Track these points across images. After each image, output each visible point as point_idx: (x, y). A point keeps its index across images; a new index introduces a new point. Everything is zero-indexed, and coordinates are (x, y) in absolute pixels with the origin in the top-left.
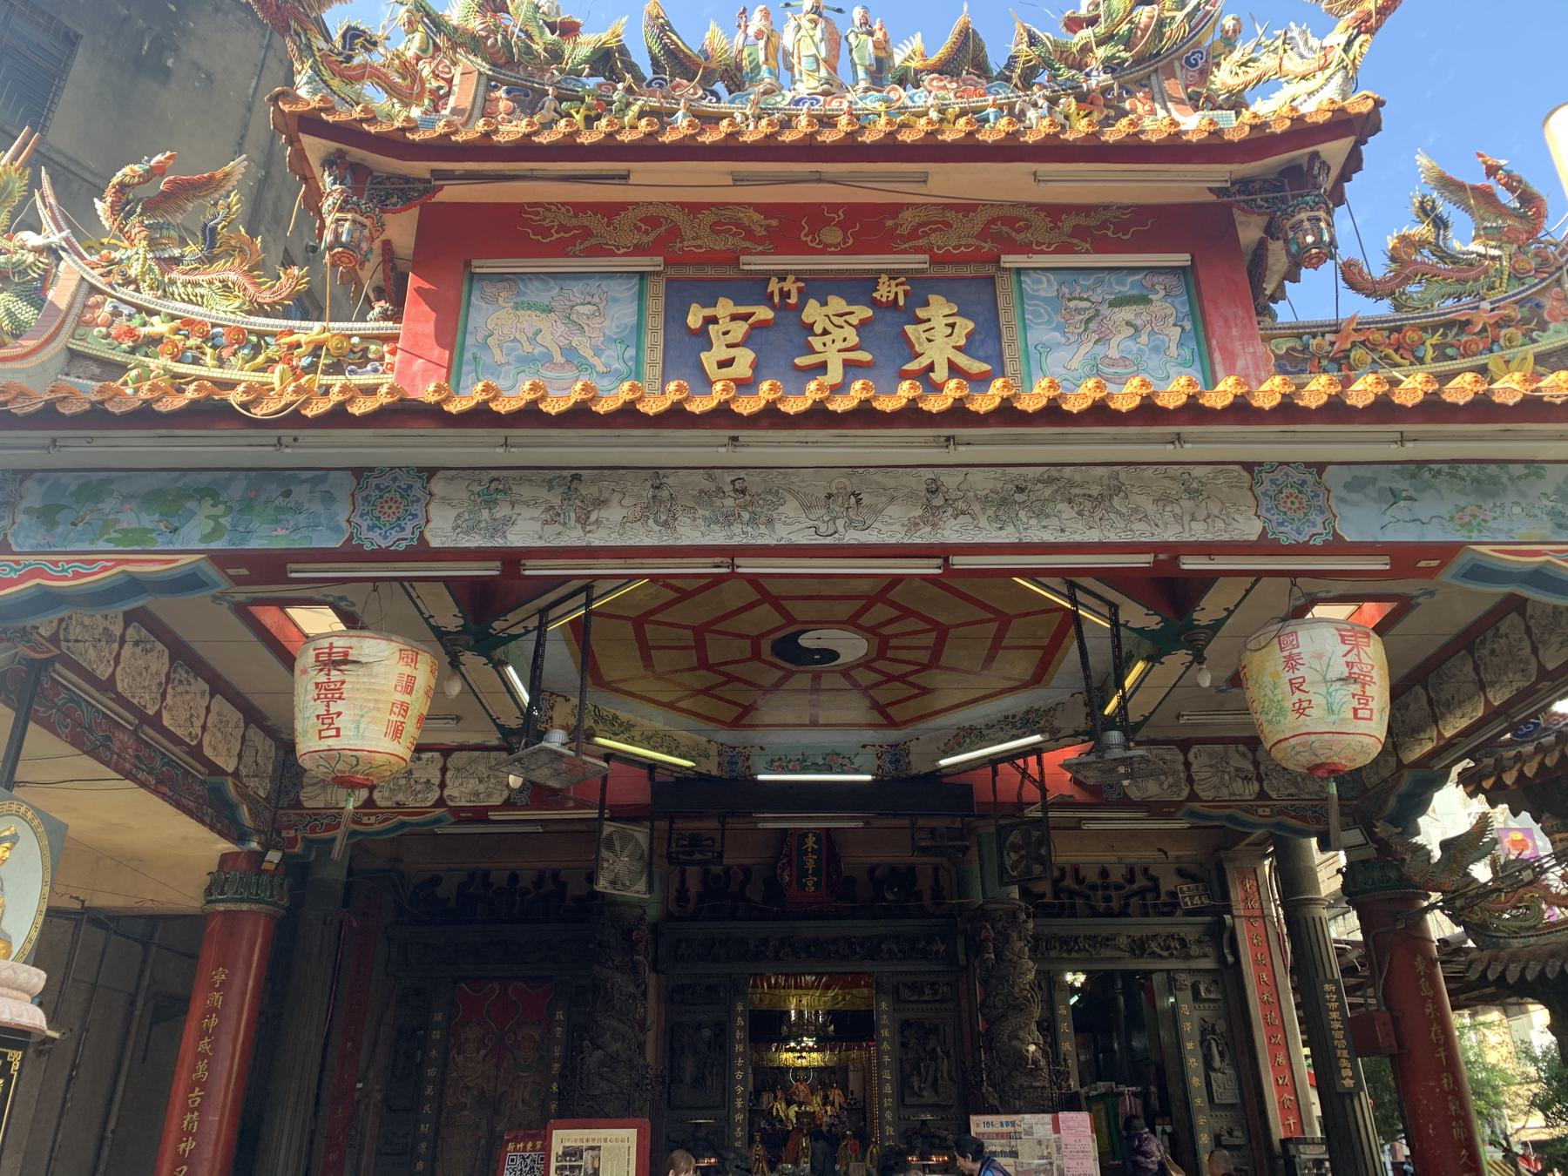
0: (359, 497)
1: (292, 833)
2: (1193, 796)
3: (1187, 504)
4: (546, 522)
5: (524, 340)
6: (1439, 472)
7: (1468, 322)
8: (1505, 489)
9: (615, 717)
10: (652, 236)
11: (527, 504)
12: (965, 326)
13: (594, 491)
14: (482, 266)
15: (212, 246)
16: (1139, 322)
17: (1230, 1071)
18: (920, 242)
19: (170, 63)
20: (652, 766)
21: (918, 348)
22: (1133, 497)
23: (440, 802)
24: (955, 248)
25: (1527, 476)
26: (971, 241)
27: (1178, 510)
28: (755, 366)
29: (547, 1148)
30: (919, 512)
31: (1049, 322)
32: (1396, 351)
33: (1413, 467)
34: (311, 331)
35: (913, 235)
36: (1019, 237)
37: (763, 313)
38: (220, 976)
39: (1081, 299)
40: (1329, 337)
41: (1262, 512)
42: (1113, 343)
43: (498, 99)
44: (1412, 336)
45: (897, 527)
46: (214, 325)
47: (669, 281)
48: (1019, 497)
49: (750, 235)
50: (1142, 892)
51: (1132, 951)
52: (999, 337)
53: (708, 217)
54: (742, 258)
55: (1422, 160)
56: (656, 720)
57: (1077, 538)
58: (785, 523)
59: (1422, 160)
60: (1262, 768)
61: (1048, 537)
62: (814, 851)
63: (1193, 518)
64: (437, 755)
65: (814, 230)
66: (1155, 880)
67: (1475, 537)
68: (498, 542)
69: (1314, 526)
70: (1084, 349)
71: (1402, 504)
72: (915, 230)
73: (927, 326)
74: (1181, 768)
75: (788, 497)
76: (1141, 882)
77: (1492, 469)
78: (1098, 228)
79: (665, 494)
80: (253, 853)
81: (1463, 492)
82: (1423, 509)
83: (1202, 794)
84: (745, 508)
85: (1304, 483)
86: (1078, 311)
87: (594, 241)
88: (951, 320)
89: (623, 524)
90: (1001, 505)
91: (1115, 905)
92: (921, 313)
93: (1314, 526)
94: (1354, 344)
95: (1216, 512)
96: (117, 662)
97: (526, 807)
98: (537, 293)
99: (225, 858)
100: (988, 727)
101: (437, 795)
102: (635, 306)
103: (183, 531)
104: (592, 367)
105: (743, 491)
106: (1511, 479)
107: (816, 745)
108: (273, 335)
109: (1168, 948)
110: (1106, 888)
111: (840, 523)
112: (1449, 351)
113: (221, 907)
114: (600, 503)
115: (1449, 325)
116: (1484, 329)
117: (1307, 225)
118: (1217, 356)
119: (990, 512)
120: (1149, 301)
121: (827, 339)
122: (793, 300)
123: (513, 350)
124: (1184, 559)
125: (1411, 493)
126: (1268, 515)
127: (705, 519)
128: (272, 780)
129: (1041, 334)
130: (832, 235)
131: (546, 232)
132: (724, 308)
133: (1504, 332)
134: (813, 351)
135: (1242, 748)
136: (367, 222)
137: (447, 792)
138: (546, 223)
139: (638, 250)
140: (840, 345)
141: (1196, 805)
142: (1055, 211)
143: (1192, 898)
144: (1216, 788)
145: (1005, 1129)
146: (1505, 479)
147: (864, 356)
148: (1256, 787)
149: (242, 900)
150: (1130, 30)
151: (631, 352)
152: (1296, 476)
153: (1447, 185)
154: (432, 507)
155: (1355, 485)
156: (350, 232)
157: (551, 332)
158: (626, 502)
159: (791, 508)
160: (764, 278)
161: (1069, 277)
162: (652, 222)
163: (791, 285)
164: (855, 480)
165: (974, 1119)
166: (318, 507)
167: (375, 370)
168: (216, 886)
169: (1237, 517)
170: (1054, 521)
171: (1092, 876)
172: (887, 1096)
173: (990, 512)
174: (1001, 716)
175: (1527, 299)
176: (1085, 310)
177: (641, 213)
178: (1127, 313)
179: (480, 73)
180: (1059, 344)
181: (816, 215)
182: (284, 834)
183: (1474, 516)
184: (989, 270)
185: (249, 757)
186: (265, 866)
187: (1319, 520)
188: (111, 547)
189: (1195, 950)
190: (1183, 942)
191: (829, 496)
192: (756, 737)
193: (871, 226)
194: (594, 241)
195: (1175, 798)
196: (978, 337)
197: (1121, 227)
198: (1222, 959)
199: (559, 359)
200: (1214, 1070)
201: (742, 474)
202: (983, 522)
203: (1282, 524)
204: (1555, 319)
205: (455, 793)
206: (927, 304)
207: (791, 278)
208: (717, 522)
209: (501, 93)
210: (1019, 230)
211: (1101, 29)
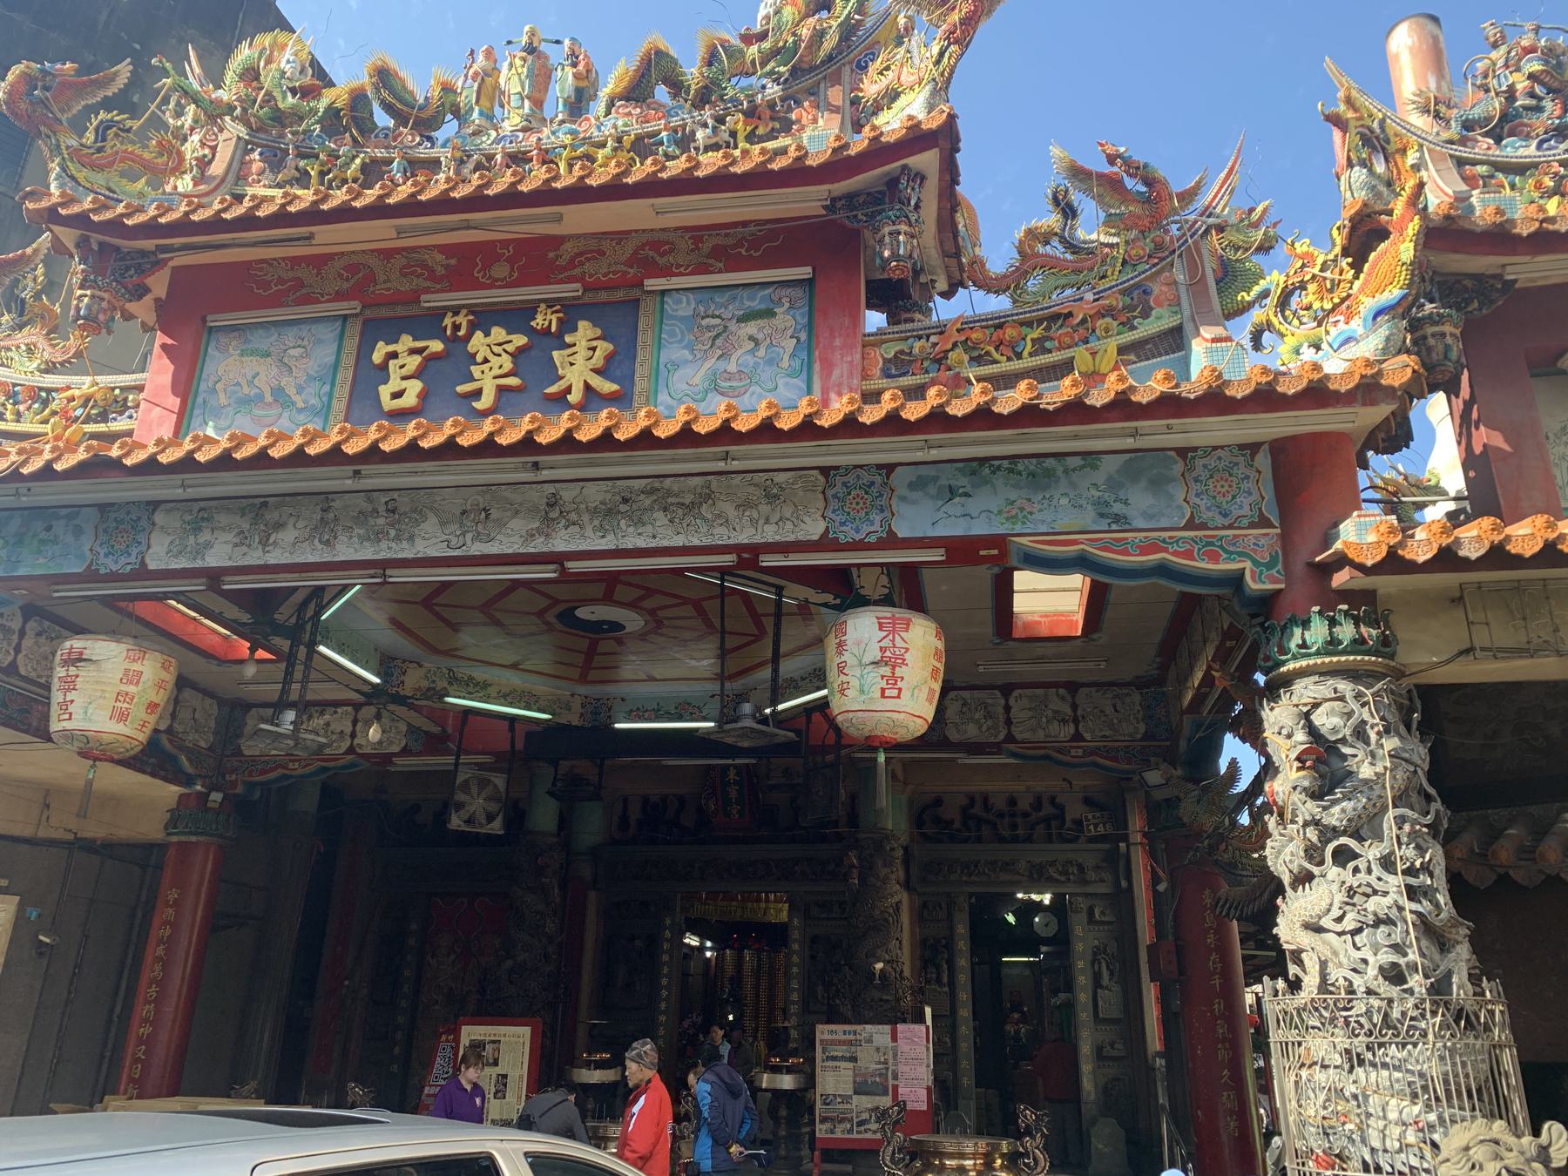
2: (1010, 738)
3: (764, 508)
4: (236, 545)
5: (244, 383)
6: (999, 468)
7: (1070, 314)
8: (1058, 480)
9: (471, 678)
11: (223, 529)
12: (604, 348)
13: (276, 515)
14: (216, 320)
15: (21, 314)
16: (760, 336)
17: (1116, 988)
19: (136, 98)
20: (513, 719)
22: (720, 504)
23: (351, 750)
24: (605, 275)
25: (1083, 467)
27: (755, 515)
28: (423, 396)
29: (457, 1040)
31: (680, 341)
32: (997, 348)
33: (975, 464)
34: (84, 384)
35: (571, 264)
37: (436, 346)
38: (173, 895)
39: (713, 317)
40: (933, 339)
41: (829, 514)
42: (734, 359)
43: (251, 162)
44: (1010, 332)
45: (516, 538)
46: (15, 385)
47: (366, 322)
48: (623, 508)
49: (432, 275)
50: (1047, 820)
51: (1031, 877)
52: (635, 358)
53: (399, 261)
54: (423, 297)
55: (1055, 151)
56: (515, 680)
57: (666, 543)
58: (424, 539)
59: (1055, 151)
60: (1079, 712)
61: (641, 543)
62: (735, 782)
63: (767, 521)
64: (349, 709)
65: (486, 267)
66: (1061, 808)
67: (1018, 529)
68: (199, 564)
69: (872, 524)
70: (708, 365)
71: (957, 500)
72: (572, 260)
73: (570, 351)
74: (1001, 710)
75: (430, 514)
76: (1048, 810)
77: (1050, 462)
78: (734, 246)
79: (331, 515)
80: (199, 793)
81: (1017, 486)
82: (973, 505)
83: (1019, 737)
84: (392, 525)
85: (873, 483)
86: (709, 328)
87: (304, 291)
90: (607, 514)
91: (1020, 832)
92: (568, 339)
93: (872, 524)
94: (955, 345)
95: (788, 515)
96: (18, 650)
97: (420, 754)
98: (260, 341)
99: (182, 796)
100: (803, 679)
101: (348, 744)
102: (335, 346)
104: (293, 403)
106: (1066, 471)
107: (667, 692)
108: (57, 390)
109: (1066, 873)
110: (1013, 815)
112: (1048, 345)
113: (174, 839)
114: (279, 526)
115: (1054, 318)
116: (1084, 321)
117: (887, 240)
118: (817, 367)
119: (596, 523)
121: (486, 367)
124: (761, 558)
125: (969, 489)
126: (833, 516)
127: (359, 536)
128: (216, 733)
129: (674, 352)
131: (266, 285)
132: (406, 342)
133: (1099, 323)
134: (473, 380)
135: (1062, 691)
136: (106, 295)
137: (356, 741)
138: (268, 277)
139: (340, 296)
140: (497, 372)
141: (1012, 746)
142: (697, 233)
143: (1096, 826)
144: (1033, 730)
145: (848, 1037)
146: (1059, 472)
147: (513, 381)
148: (1071, 729)
149: (191, 833)
150: (795, 42)
151: (327, 388)
152: (866, 477)
153: (1078, 173)
154: (153, 535)
155: (918, 484)
156: (88, 307)
157: (265, 374)
158: (299, 525)
159: (430, 525)
160: (440, 313)
161: (705, 295)
162: (353, 269)
164: (488, 497)
165: (819, 1027)
166: (69, 539)
167: (131, 417)
168: (175, 819)
169: (806, 519)
170: (649, 529)
171: (999, 803)
172: (794, 1003)
173: (596, 523)
174: (810, 669)
175: (1137, 286)
176: (714, 327)
177: (344, 262)
178: (751, 328)
179: (239, 138)
180: (687, 361)
181: (487, 252)
182: (228, 777)
183: (1022, 509)
184: (636, 293)
185: (184, 714)
186: (210, 805)
187: (878, 519)
189: (1092, 875)
190: (1081, 868)
191: (464, 512)
192: (610, 689)
193: (536, 259)
194: (304, 291)
195: (992, 740)
196: (618, 358)
197: (755, 243)
198: (1117, 884)
199: (269, 399)
200: (1101, 987)
201: (395, 495)
202: (589, 532)
203: (842, 524)
204: (1159, 305)
206: (575, 329)
207: (464, 312)
208: (369, 539)
209: (256, 155)
210: (662, 255)
211: (766, 45)
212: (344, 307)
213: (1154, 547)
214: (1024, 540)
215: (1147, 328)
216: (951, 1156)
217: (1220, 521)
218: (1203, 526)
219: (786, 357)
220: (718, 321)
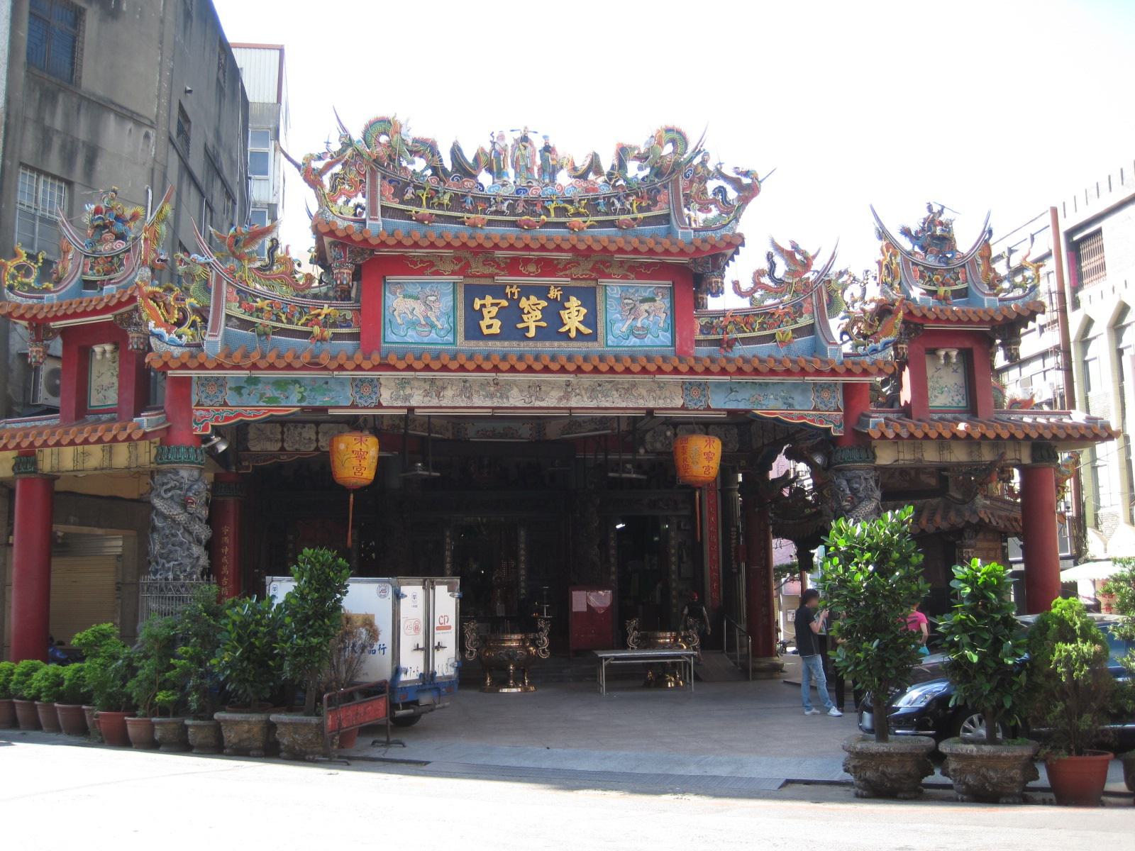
0: (354, 385)
1: (247, 464)
5: (408, 313)
7: (773, 314)
10: (459, 266)
12: (584, 311)
16: (650, 310)
18: (567, 272)
21: (565, 322)
23: (317, 449)
26: (588, 272)
30: (562, 394)
35: (565, 269)
36: (607, 271)
37: (505, 303)
39: (629, 299)
40: (721, 319)
54: (496, 278)
61: (608, 405)
63: (660, 398)
67: (755, 407)
68: (407, 404)
70: (629, 322)
72: (565, 266)
73: (568, 311)
79: (468, 385)
84: (497, 391)
86: (627, 304)
88: (578, 308)
89: (453, 397)
100: (584, 422)
101: (315, 445)
103: (291, 397)
105: (497, 384)
111: (533, 398)
120: (655, 301)
121: (529, 316)
122: (516, 297)
123: (405, 317)
130: (532, 268)
131: (415, 263)
134: (524, 322)
135: (701, 427)
137: (320, 444)
139: (453, 273)
140: (534, 319)
147: (544, 324)
158: (454, 388)
163: (515, 290)
173: (588, 395)
178: (646, 306)
182: (243, 464)
188: (265, 404)
191: (529, 387)
194: (435, 269)
195: (668, 450)
199: (423, 322)
202: (585, 399)
205: (324, 444)
207: (515, 286)
208: (487, 397)
210: (607, 267)
212: (456, 278)
213: (802, 417)
214: (757, 412)
215: (804, 321)
216: (662, 638)
217: (824, 408)
218: (819, 410)
219: (662, 322)
220: (631, 301)
